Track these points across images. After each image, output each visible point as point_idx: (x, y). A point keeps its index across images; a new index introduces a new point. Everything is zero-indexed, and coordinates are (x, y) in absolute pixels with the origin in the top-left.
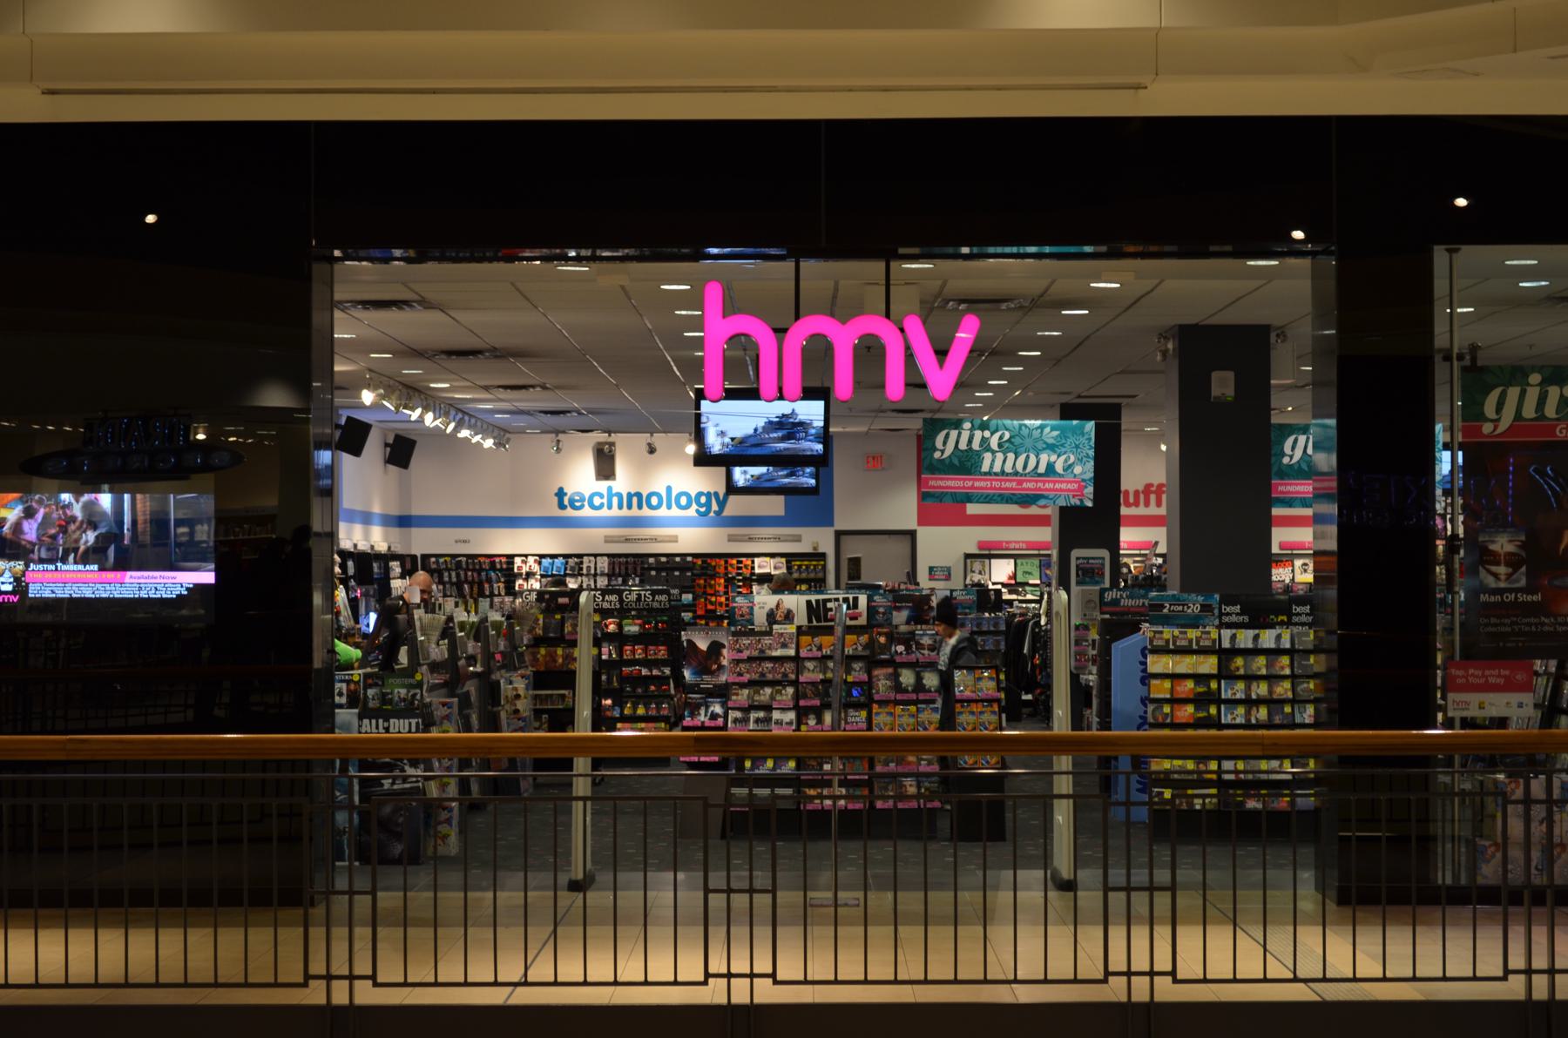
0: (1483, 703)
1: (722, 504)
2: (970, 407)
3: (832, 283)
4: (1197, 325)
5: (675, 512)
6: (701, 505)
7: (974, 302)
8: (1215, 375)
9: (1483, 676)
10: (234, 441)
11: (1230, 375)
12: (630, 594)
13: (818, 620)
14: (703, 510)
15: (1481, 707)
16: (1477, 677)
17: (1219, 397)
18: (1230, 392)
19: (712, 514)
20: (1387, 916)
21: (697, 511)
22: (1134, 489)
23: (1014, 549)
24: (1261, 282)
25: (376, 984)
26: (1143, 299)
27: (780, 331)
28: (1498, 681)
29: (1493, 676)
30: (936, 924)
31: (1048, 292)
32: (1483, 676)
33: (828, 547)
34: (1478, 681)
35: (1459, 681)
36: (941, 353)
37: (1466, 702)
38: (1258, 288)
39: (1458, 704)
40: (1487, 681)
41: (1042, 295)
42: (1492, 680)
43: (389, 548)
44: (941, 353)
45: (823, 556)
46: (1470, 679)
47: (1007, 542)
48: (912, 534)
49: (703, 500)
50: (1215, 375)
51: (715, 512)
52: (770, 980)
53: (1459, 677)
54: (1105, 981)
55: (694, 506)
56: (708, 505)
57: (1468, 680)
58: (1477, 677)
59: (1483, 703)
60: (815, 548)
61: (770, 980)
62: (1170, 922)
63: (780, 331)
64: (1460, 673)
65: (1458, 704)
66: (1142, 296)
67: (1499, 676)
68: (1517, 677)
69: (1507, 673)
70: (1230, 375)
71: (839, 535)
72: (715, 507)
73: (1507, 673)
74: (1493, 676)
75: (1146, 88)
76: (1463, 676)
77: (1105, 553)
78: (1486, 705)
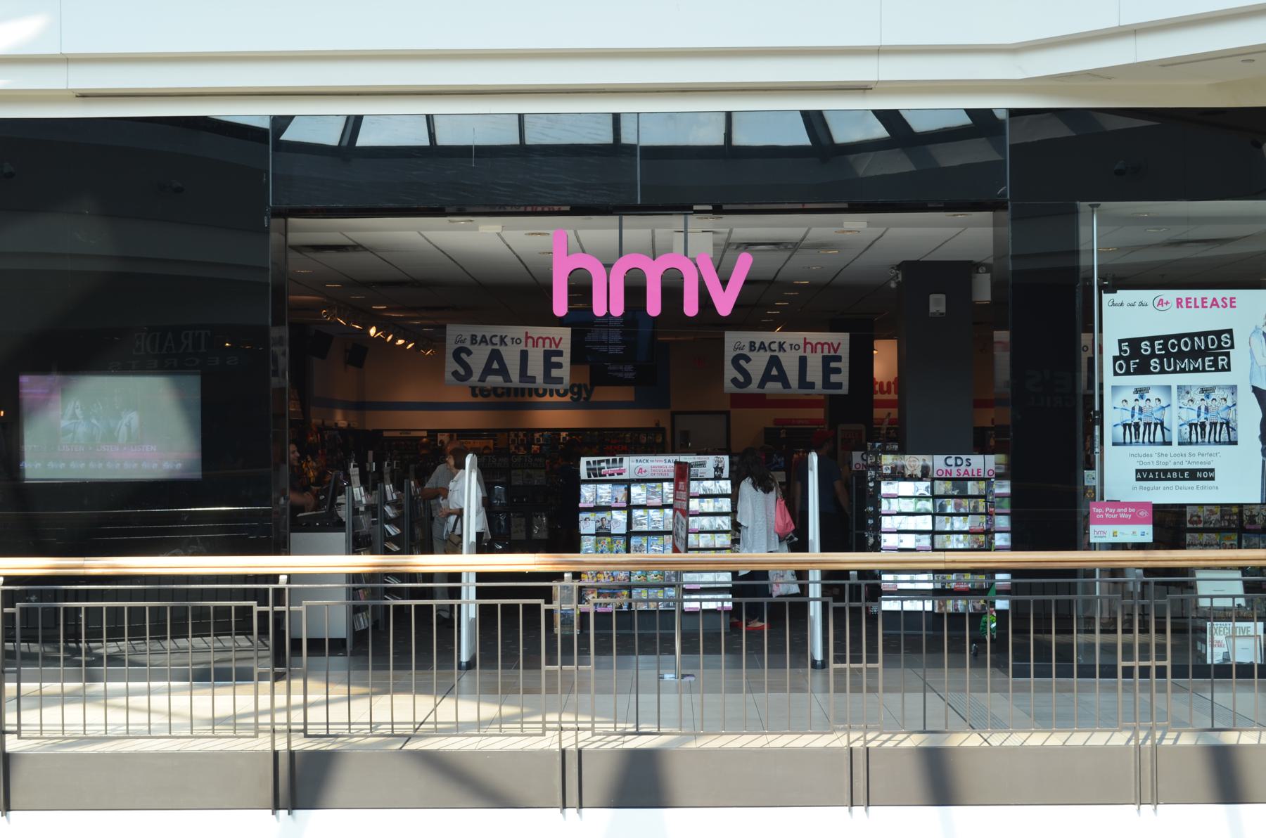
0: (1116, 532)
1: (589, 393)
2: (764, 322)
3: (650, 231)
4: (918, 261)
5: (556, 398)
6: (573, 393)
7: (748, 245)
8: (933, 297)
9: (1116, 513)
10: (413, 347)
11: (943, 297)
12: (516, 458)
13: (595, 476)
14: (575, 397)
15: (1115, 535)
16: (1111, 513)
17: (934, 313)
18: (943, 309)
19: (582, 400)
20: (1215, 689)
21: (571, 397)
22: (887, 381)
23: (801, 424)
24: (959, 229)
25: (19, 738)
26: (876, 242)
27: (608, 266)
28: (1127, 516)
29: (1123, 513)
30: (131, 696)
31: (807, 237)
32: (1116, 513)
33: (665, 424)
34: (1112, 516)
35: (1099, 516)
36: (724, 283)
37: (1103, 532)
38: (958, 233)
39: (1098, 533)
40: (1118, 516)
41: (802, 240)
42: (1122, 516)
43: (349, 425)
44: (724, 283)
45: (663, 429)
46: (1107, 515)
47: (795, 419)
48: (727, 413)
49: (576, 390)
50: (933, 297)
51: (584, 398)
52: (302, 734)
53: (1098, 513)
54: (543, 734)
55: (569, 395)
56: (579, 393)
57: (1105, 516)
58: (1111, 513)
59: (1116, 532)
60: (657, 424)
61: (302, 734)
62: (253, 693)
63: (608, 266)
64: (1099, 510)
65: (1098, 533)
66: (876, 240)
67: (1128, 513)
68: (1140, 514)
69: (1134, 510)
70: (943, 297)
71: (673, 414)
72: (584, 395)
73: (1134, 510)
74: (1123, 513)
75: (871, 89)
76: (1101, 513)
77: (862, 427)
78: (1118, 534)
